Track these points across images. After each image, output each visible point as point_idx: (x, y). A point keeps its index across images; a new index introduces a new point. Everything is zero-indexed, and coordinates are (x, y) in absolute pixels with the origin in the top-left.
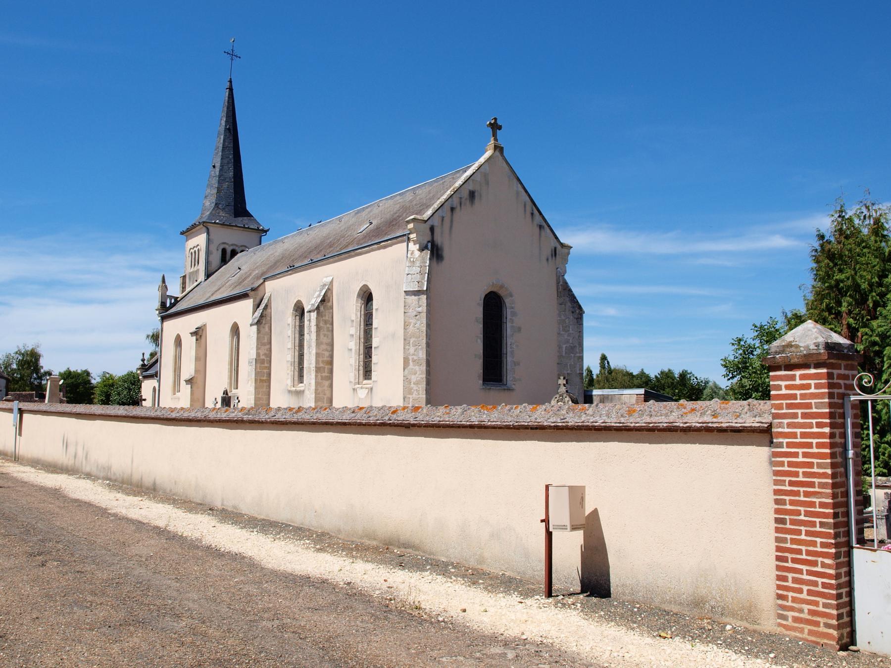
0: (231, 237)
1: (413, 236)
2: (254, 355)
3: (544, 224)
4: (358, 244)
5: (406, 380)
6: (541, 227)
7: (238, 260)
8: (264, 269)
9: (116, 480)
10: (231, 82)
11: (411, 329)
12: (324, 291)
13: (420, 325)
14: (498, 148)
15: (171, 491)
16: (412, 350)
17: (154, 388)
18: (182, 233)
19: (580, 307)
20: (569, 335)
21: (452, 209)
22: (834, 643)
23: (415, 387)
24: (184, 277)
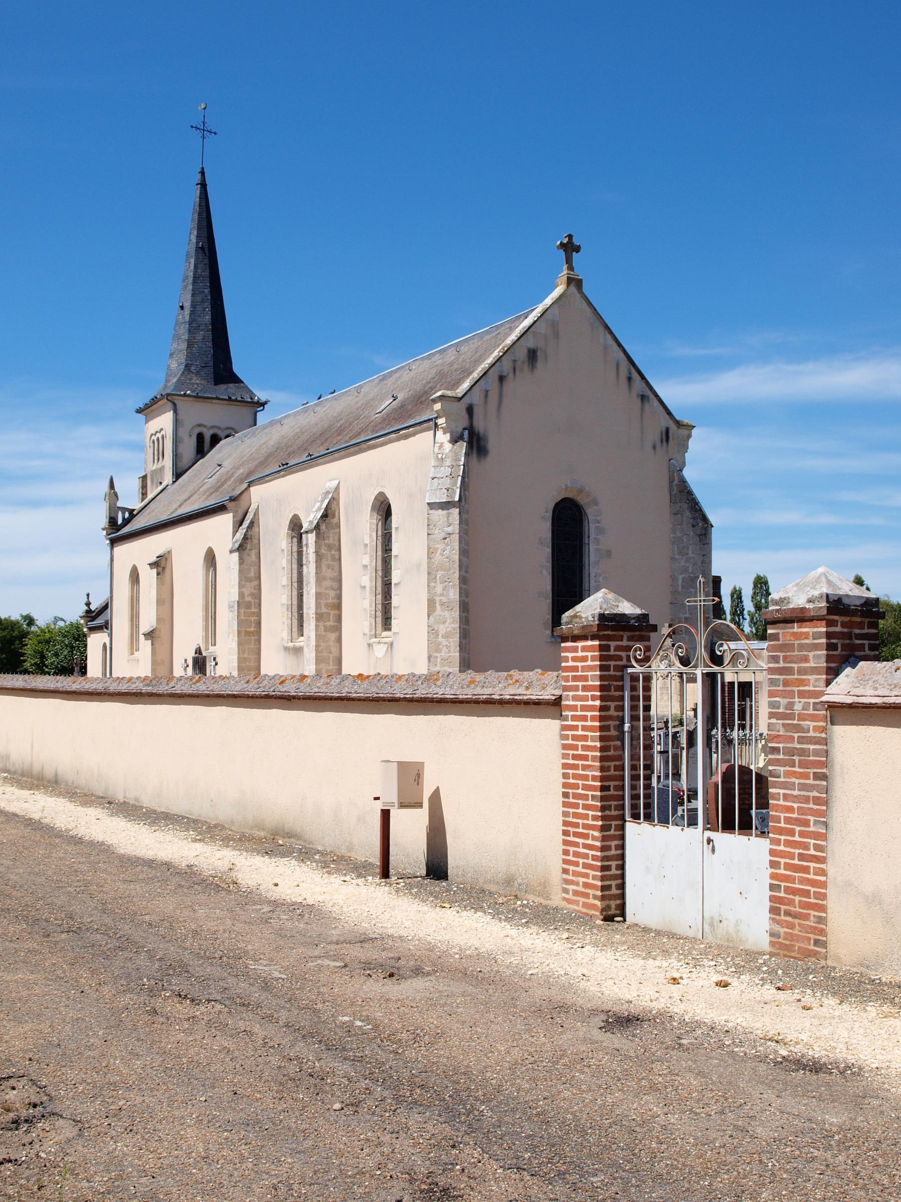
0: (211, 415)
1: (441, 421)
2: (236, 597)
3: (649, 393)
4: (373, 431)
5: (432, 632)
6: (643, 398)
7: (220, 451)
8: (251, 466)
9: (15, 773)
10: (202, 173)
11: (438, 558)
12: (326, 502)
13: (452, 550)
14: (574, 282)
15: (73, 783)
16: (439, 589)
17: (105, 646)
18: (139, 411)
19: (705, 519)
20: (687, 561)
21: (502, 379)
22: (598, 913)
23: (445, 642)
24: (144, 478)
